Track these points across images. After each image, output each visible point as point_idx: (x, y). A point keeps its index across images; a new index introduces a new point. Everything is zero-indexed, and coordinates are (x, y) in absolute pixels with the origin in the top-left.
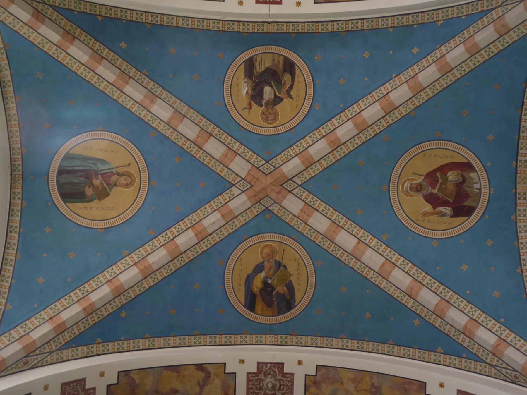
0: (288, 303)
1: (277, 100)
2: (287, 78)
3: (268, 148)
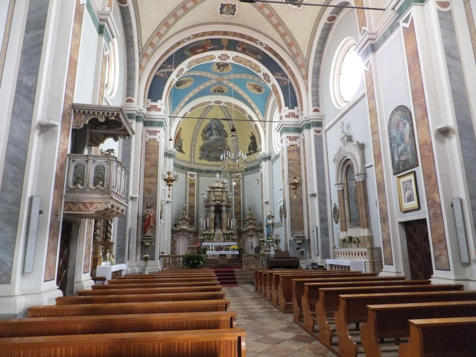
0: (223, 91)
1: (223, 69)
2: (226, 66)
3: (221, 75)
